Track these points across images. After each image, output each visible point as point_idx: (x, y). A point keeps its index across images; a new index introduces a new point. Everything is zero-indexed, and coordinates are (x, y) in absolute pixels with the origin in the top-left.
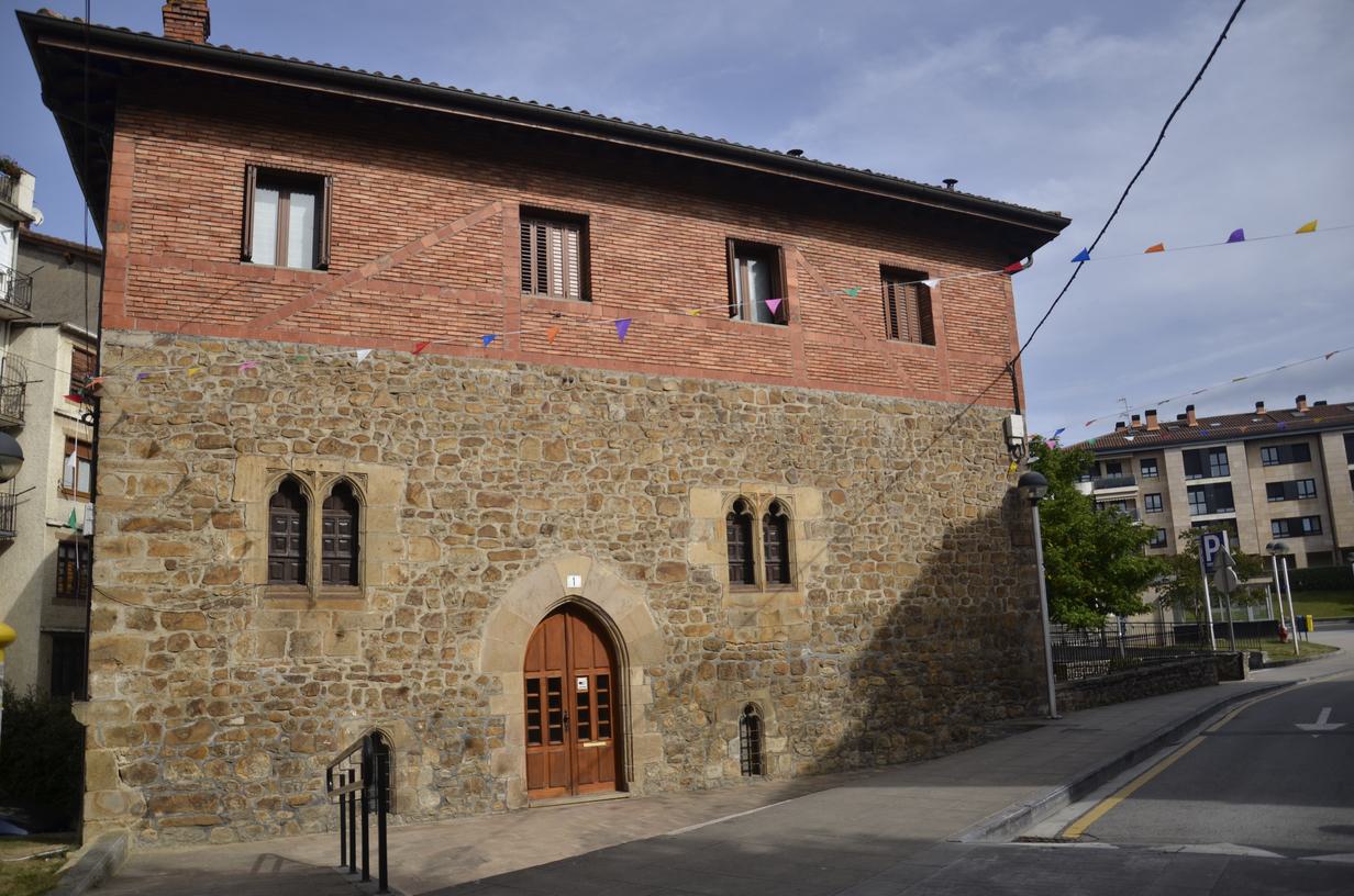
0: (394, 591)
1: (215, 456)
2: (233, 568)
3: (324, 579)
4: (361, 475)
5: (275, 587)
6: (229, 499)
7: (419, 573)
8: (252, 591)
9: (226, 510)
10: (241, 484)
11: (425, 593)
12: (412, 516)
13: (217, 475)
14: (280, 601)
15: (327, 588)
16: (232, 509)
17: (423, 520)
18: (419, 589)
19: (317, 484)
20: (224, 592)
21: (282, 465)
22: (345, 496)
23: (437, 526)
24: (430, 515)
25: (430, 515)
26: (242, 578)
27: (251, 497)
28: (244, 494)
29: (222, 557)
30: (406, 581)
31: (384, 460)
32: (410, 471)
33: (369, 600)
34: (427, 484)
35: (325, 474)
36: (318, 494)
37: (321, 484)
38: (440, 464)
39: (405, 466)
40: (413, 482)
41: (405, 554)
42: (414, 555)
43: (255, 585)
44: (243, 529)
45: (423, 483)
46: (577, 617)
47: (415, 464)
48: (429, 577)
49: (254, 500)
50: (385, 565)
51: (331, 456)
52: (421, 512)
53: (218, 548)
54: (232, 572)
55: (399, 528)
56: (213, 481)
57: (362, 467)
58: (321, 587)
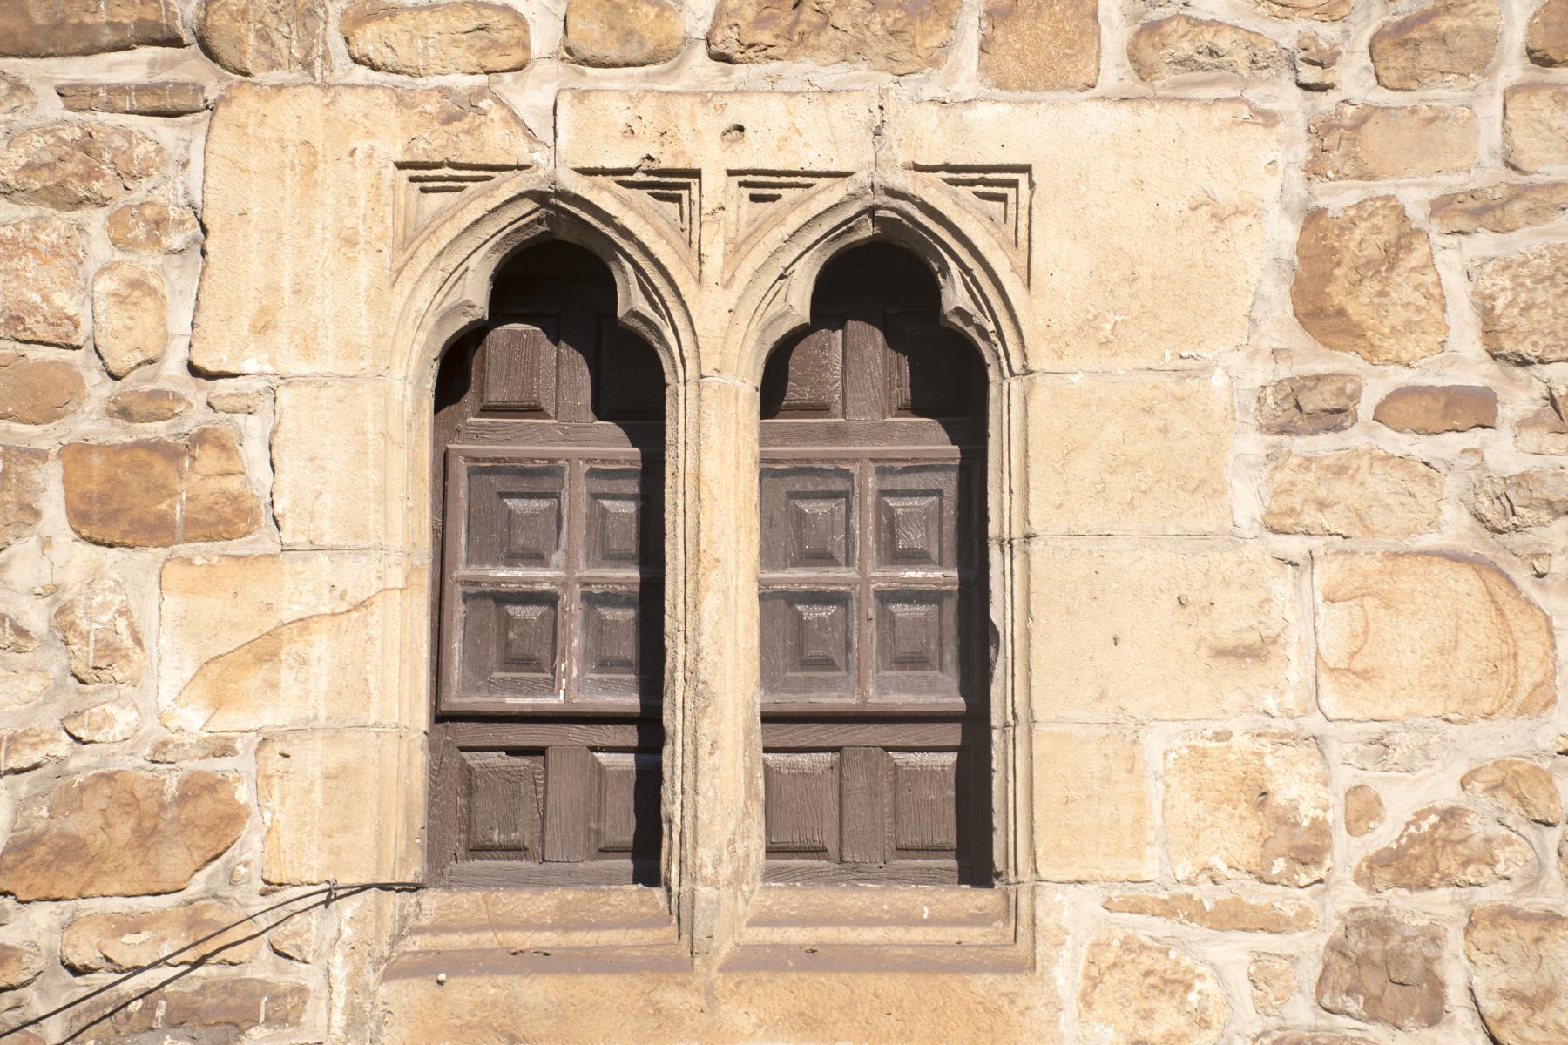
0: (1230, 918)
1: (72, 95)
2: (198, 788)
3: (772, 851)
4: (994, 180)
5: (466, 901)
6: (173, 367)
7: (1403, 804)
8: (314, 928)
9: (158, 430)
10: (242, 261)
11: (1455, 940)
12: (1335, 418)
13: (95, 218)
14: (490, 988)
15: (788, 898)
16: (195, 418)
17: (1421, 447)
18: (1411, 908)
19: (714, 252)
20: (130, 948)
21: (495, 141)
22: (891, 290)
23: (1522, 479)
24: (1473, 408)
25: (1473, 408)
26: (250, 848)
27: (307, 348)
28: (263, 327)
29: (123, 720)
30: (1309, 851)
31: (1142, 70)
32: (1321, 130)
33: (1063, 974)
34: (1441, 207)
35: (762, 186)
36: (723, 303)
37: (736, 249)
38: (1538, 58)
39: (1286, 97)
40: (1339, 198)
41: (1296, 671)
42: (1356, 673)
43: (332, 896)
44: (262, 540)
45: (1415, 199)
46: (571, 343)
47: (1354, 80)
48: (1479, 826)
49: (326, 364)
50: (1158, 746)
51: (795, 71)
52: (1401, 393)
53: (101, 665)
54: (195, 814)
55: (1246, 503)
56: (69, 252)
57: (996, 129)
58: (760, 896)
